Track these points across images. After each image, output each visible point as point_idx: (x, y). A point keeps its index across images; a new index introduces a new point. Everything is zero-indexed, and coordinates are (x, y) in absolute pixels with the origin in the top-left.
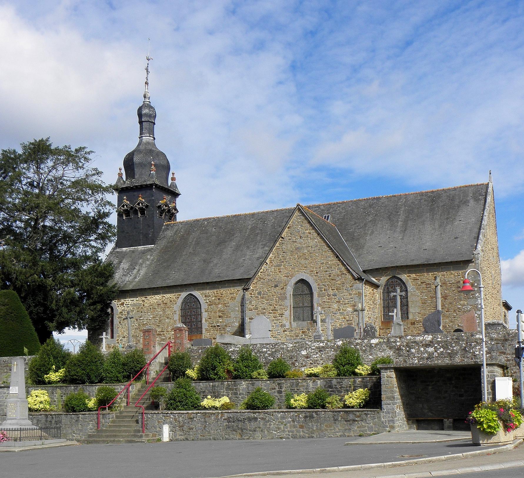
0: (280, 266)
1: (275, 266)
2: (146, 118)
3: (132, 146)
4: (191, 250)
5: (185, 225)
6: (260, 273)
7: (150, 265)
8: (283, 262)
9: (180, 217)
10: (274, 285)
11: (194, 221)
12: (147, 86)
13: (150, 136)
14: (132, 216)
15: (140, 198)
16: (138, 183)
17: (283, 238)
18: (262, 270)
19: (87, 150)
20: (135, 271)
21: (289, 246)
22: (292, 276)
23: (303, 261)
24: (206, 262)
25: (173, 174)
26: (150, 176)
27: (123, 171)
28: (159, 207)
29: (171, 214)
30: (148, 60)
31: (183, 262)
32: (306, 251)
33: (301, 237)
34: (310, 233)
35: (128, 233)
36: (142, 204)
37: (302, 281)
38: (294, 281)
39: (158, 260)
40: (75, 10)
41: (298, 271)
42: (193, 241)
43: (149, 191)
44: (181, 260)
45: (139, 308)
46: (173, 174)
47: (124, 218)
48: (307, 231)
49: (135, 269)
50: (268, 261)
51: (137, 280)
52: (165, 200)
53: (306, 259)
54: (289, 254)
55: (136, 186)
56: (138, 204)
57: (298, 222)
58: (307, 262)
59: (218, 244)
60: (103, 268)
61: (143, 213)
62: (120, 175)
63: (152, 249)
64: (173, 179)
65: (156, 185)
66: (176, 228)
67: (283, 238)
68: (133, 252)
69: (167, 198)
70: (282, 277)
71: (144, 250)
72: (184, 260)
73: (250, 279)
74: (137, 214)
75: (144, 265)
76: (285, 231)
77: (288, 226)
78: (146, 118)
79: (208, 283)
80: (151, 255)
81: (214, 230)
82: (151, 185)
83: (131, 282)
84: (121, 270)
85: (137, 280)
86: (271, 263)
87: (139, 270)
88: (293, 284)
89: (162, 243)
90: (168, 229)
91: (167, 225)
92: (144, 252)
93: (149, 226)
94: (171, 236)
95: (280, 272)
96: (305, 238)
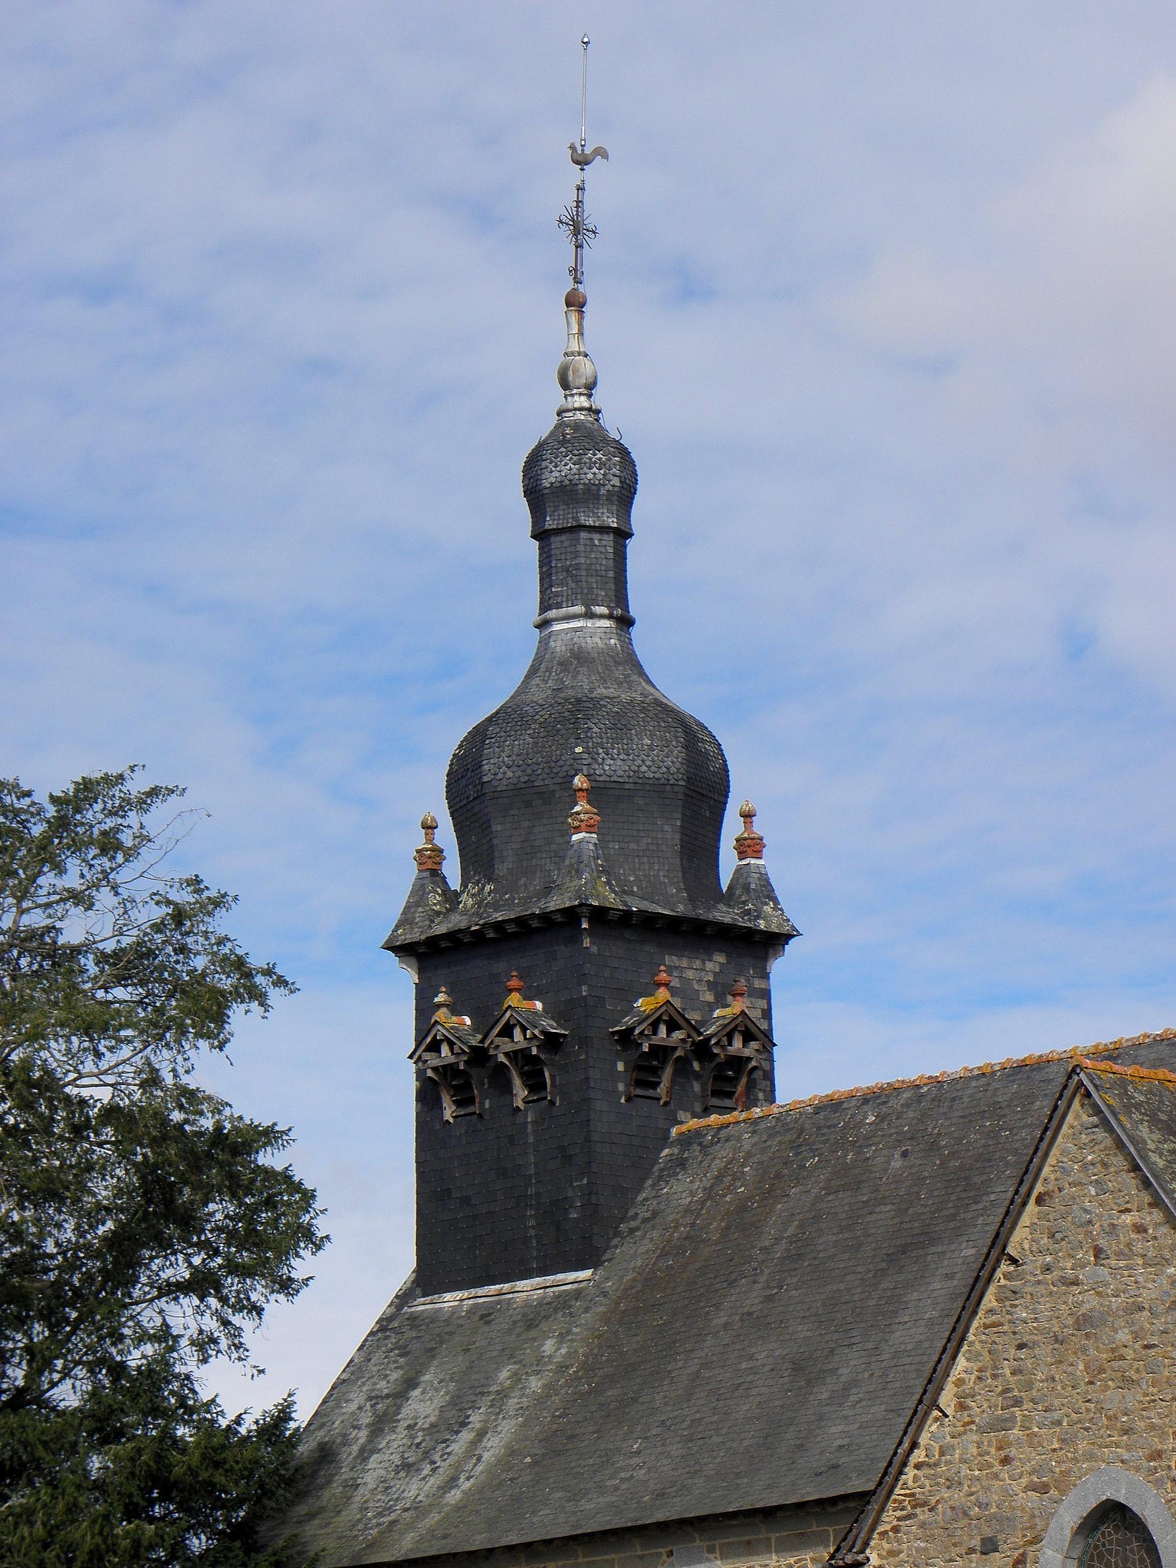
0: (1002, 1425)
1: (981, 1431)
2: (579, 506)
3: (494, 685)
5: (772, 1133)
6: (910, 1473)
7: (540, 1400)
8: (1018, 1403)
9: (805, 1071)
10: (976, 1542)
11: (818, 1110)
12: (574, 318)
13: (589, 615)
15: (514, 999)
16: (510, 904)
17: (1014, 1261)
18: (918, 1455)
19: (136, 786)
20: (459, 1445)
21: (1044, 1306)
22: (1063, 1484)
23: (1113, 1398)
24: (805, 1371)
25: (748, 816)
26: (588, 861)
27: (447, 837)
28: (626, 1038)
29: (733, 1068)
30: (582, 161)
31: (697, 1374)
32: (1123, 1336)
33: (1098, 1252)
34: (1140, 1229)
35: (466, 1200)
37: (1113, 1516)
38: (1070, 1514)
39: (588, 1368)
41: (1090, 1457)
42: (778, 1240)
43: (562, 951)
46: (748, 816)
47: (448, 1115)
48: (1128, 1219)
49: (464, 1424)
50: (947, 1399)
51: (454, 1496)
52: (663, 994)
53: (1127, 1382)
54: (1045, 1352)
55: (498, 926)
57: (1085, 1167)
58: (1133, 1398)
59: (891, 1259)
60: (195, 1460)
61: (535, 1084)
62: (430, 861)
63: (577, 1294)
64: (749, 846)
65: (599, 915)
66: (723, 1152)
67: (1014, 1261)
68: (485, 1315)
69: (698, 971)
70: (1014, 1490)
71: (541, 1302)
72: (706, 1365)
73: (864, 1497)
74: (507, 1089)
75: (512, 1403)
76: (1025, 1219)
77: (1039, 1188)
78: (579, 506)
79: (768, 1514)
80: (561, 1338)
81: (897, 1163)
82: (571, 915)
83: (419, 1509)
84: (401, 1431)
85: (454, 1496)
86: (962, 1407)
87: (481, 1434)
88: (1068, 1533)
89: (633, 1255)
91: (686, 1140)
92: (534, 1318)
93: (568, 1159)
95: (1006, 1461)
96: (1119, 1254)
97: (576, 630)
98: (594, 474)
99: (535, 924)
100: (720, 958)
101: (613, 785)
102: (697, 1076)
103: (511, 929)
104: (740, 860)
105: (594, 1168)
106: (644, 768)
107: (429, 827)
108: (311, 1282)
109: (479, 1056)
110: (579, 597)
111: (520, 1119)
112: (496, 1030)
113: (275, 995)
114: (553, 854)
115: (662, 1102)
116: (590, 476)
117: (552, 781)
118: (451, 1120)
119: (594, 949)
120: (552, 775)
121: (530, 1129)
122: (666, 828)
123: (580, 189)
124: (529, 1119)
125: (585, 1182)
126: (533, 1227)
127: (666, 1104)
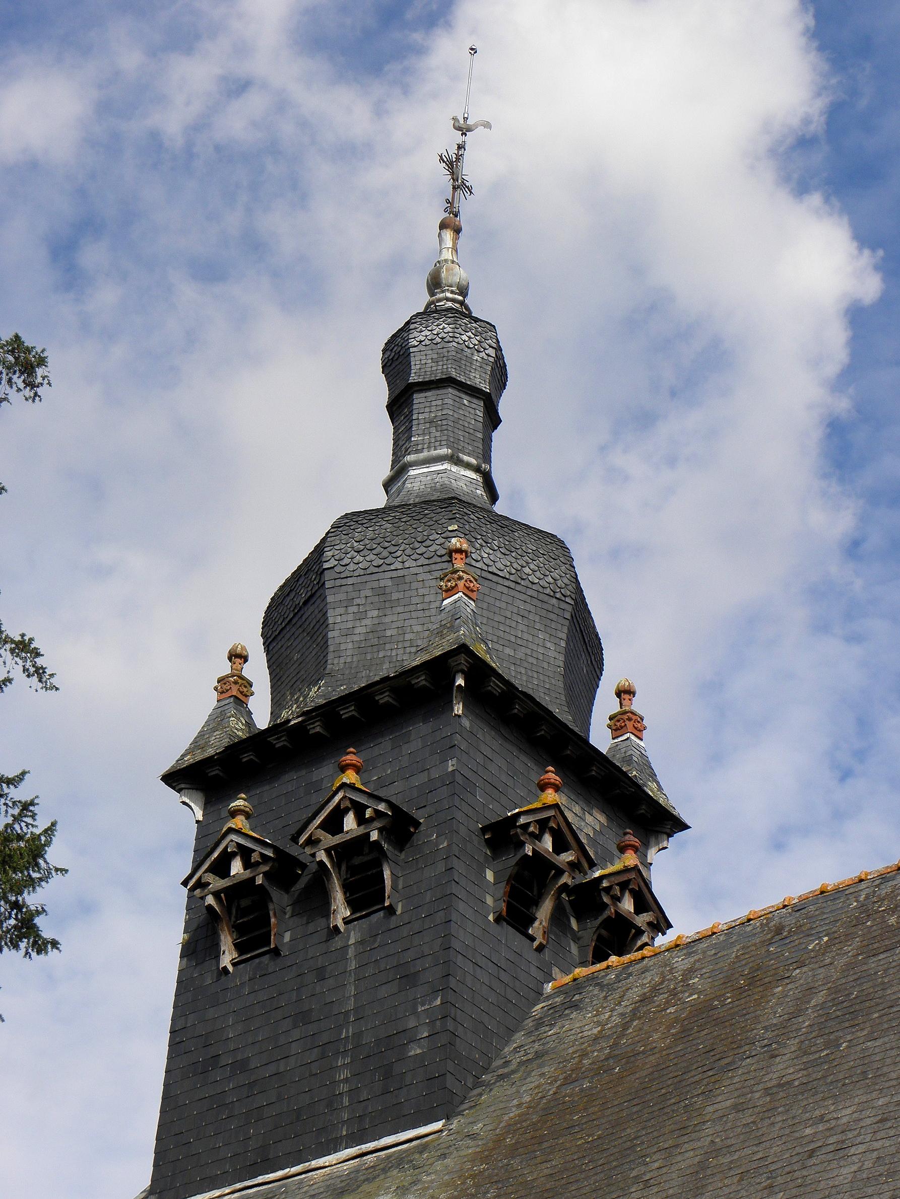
4: (785, 1067)
14: (284, 935)
27: (258, 671)
30: (464, 130)
31: (702, 1166)
36: (359, 809)
40: (27, 933)
44: (687, 1159)
45: (260, 963)
47: (226, 960)
56: (334, 824)
61: (366, 896)
62: (234, 691)
71: (357, 1171)
72: (716, 1152)
74: (325, 910)
90: (575, 1006)
94: (596, 1039)
97: (438, 473)
98: (470, 338)
99: (384, 698)
100: (602, 818)
101: (490, 576)
102: (576, 939)
103: (349, 712)
104: (613, 739)
105: (453, 983)
106: (527, 570)
107: (238, 656)
108: (27, 776)
109: (284, 868)
110: (444, 443)
111: (338, 942)
112: (318, 821)
113: (45, 354)
114: (407, 644)
115: (536, 944)
116: (465, 337)
117: (414, 564)
118: (230, 968)
119: (466, 723)
120: (415, 556)
121: (351, 952)
122: (548, 645)
123: (460, 147)
124: (352, 941)
125: (438, 1002)
126: (346, 1080)
127: (540, 948)
